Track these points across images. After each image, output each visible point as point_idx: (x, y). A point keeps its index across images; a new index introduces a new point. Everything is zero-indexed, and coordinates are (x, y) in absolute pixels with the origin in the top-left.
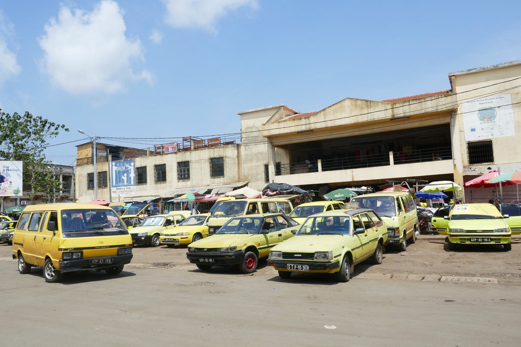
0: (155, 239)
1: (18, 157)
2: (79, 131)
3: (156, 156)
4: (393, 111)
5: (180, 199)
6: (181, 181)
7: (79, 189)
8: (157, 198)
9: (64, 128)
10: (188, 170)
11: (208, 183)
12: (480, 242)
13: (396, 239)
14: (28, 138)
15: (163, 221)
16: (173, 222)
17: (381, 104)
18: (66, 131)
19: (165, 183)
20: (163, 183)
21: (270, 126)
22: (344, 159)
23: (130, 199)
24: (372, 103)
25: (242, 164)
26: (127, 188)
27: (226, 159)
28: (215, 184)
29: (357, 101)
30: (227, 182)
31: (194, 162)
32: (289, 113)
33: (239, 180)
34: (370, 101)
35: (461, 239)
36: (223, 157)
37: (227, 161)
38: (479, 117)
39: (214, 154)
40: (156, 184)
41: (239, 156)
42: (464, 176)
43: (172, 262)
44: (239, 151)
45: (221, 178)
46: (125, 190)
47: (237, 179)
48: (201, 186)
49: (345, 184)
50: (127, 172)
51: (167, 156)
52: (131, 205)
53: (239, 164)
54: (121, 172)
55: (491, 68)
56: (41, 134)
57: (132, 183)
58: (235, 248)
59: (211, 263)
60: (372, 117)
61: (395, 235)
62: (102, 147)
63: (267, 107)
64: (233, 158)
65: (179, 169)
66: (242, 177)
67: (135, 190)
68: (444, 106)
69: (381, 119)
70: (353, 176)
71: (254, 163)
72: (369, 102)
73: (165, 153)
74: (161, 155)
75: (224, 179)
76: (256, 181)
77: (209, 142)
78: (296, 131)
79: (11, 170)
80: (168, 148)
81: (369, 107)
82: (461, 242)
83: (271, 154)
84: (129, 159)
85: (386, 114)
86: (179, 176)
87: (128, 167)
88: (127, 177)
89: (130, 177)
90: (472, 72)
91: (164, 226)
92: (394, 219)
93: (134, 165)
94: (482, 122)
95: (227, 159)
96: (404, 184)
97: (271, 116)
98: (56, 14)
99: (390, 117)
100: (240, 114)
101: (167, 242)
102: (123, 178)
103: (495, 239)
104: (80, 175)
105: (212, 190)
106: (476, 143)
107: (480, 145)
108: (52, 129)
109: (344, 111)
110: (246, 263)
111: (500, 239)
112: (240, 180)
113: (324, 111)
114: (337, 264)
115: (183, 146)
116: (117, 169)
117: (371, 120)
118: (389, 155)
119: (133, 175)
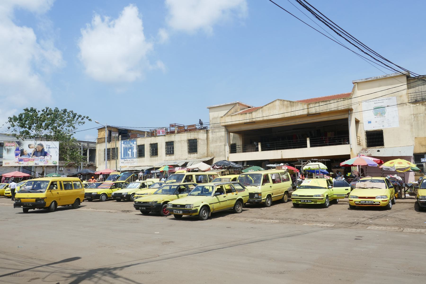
1: (56, 138)
2: (95, 122)
4: (308, 110)
7: (99, 160)
8: (151, 167)
9: (88, 119)
10: (173, 148)
11: (186, 157)
12: (306, 202)
13: (259, 200)
14: (63, 125)
15: (139, 185)
16: (146, 186)
17: (300, 104)
18: (89, 121)
21: (226, 118)
22: (276, 143)
23: (133, 168)
24: (294, 103)
25: (210, 145)
26: (131, 160)
29: (284, 102)
30: (199, 157)
32: (243, 107)
33: (207, 156)
34: (293, 102)
35: (296, 200)
37: (199, 142)
38: (374, 113)
39: (190, 137)
40: (151, 157)
41: (207, 138)
43: (131, 210)
45: (195, 154)
46: (130, 161)
47: (206, 155)
49: (280, 160)
50: (131, 148)
53: (207, 144)
54: (127, 148)
55: (382, 77)
56: (73, 122)
57: (135, 156)
58: (156, 202)
59: (144, 210)
61: (258, 197)
62: (116, 130)
63: (227, 104)
64: (203, 140)
66: (209, 153)
67: (137, 161)
68: (343, 107)
70: (282, 155)
72: (292, 103)
73: (157, 135)
74: (154, 137)
76: (219, 157)
79: (51, 148)
81: (292, 106)
82: (296, 202)
83: (227, 139)
84: (133, 139)
87: (132, 145)
88: (131, 152)
89: (133, 152)
90: (368, 80)
91: (139, 188)
92: (258, 188)
93: (136, 143)
95: (199, 141)
97: (229, 111)
98: (90, 20)
100: (209, 108)
102: (129, 152)
103: (314, 201)
104: (99, 150)
105: (188, 162)
106: (371, 132)
107: (370, 134)
108: (80, 119)
109: (276, 109)
110: (164, 211)
111: (316, 201)
113: (262, 109)
114: (196, 211)
115: (170, 130)
116: (125, 146)
118: (306, 140)
119: (135, 151)
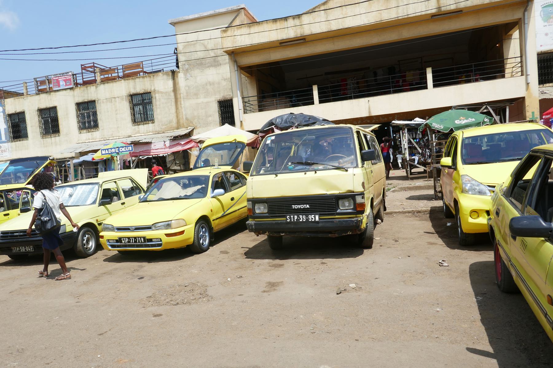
0: (85, 238)
3: (38, 96)
5: (115, 148)
6: (85, 131)
10: (95, 114)
15: (96, 193)
19: (59, 136)
20: (55, 137)
25: (182, 102)
27: (155, 95)
28: (140, 134)
31: (103, 102)
36: (150, 93)
37: (157, 98)
39: (135, 88)
40: (43, 138)
42: (540, 101)
44: (176, 82)
47: (174, 124)
48: (118, 138)
51: (58, 93)
52: (9, 164)
60: (405, 11)
64: (166, 93)
65: (80, 114)
66: (183, 121)
67: (10, 149)
69: (419, 14)
70: (369, 108)
71: (202, 100)
75: (154, 126)
77: (125, 71)
78: (279, 39)
80: (58, 82)
85: (428, 6)
86: (80, 124)
94: (546, 24)
95: (157, 95)
96: (485, 111)
99: (434, 11)
101: (125, 246)
112: (180, 125)
117: (404, 17)
